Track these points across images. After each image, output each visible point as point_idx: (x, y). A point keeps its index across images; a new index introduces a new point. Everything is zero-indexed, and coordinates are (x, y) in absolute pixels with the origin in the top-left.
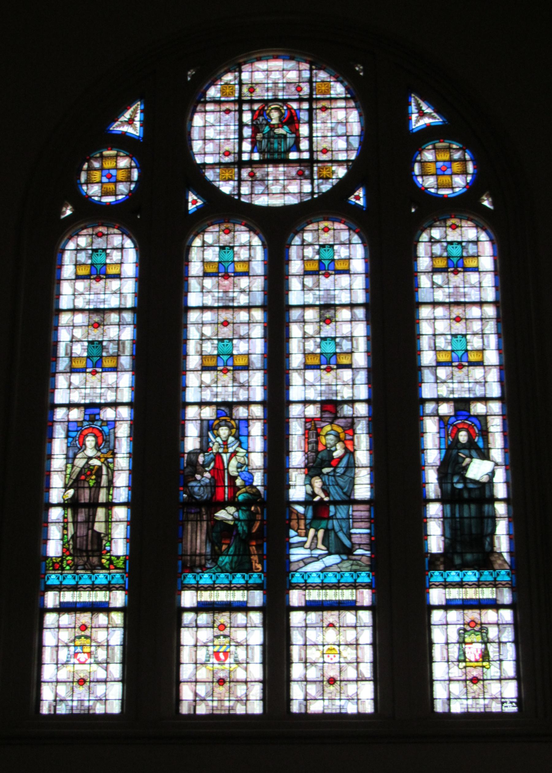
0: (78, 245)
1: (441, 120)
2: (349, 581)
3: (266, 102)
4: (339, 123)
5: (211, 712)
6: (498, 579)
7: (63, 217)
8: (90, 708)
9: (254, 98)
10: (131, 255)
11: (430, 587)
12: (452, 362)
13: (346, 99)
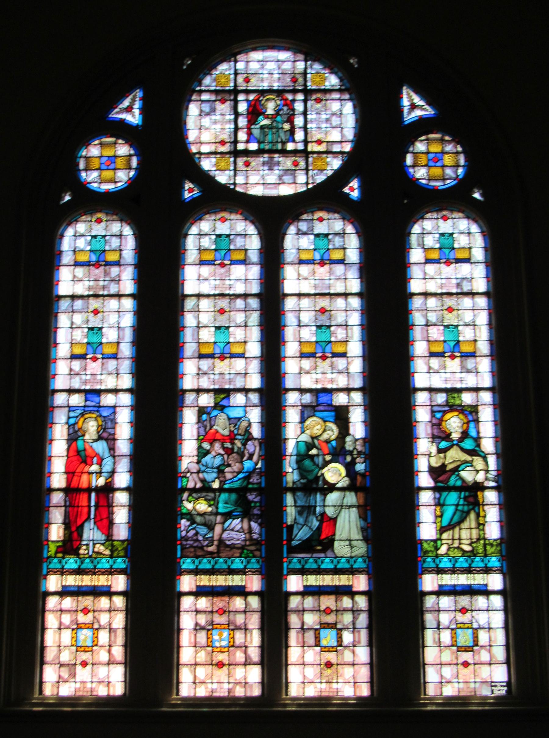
0: (200, 230)
1: (433, 113)
2: (105, 567)
3: (262, 92)
4: (333, 114)
5: (319, 694)
6: (473, 565)
7: (62, 202)
8: (339, 690)
9: (297, 88)
10: (130, 243)
11: (423, 573)
12: (444, 353)
13: (340, 91)
